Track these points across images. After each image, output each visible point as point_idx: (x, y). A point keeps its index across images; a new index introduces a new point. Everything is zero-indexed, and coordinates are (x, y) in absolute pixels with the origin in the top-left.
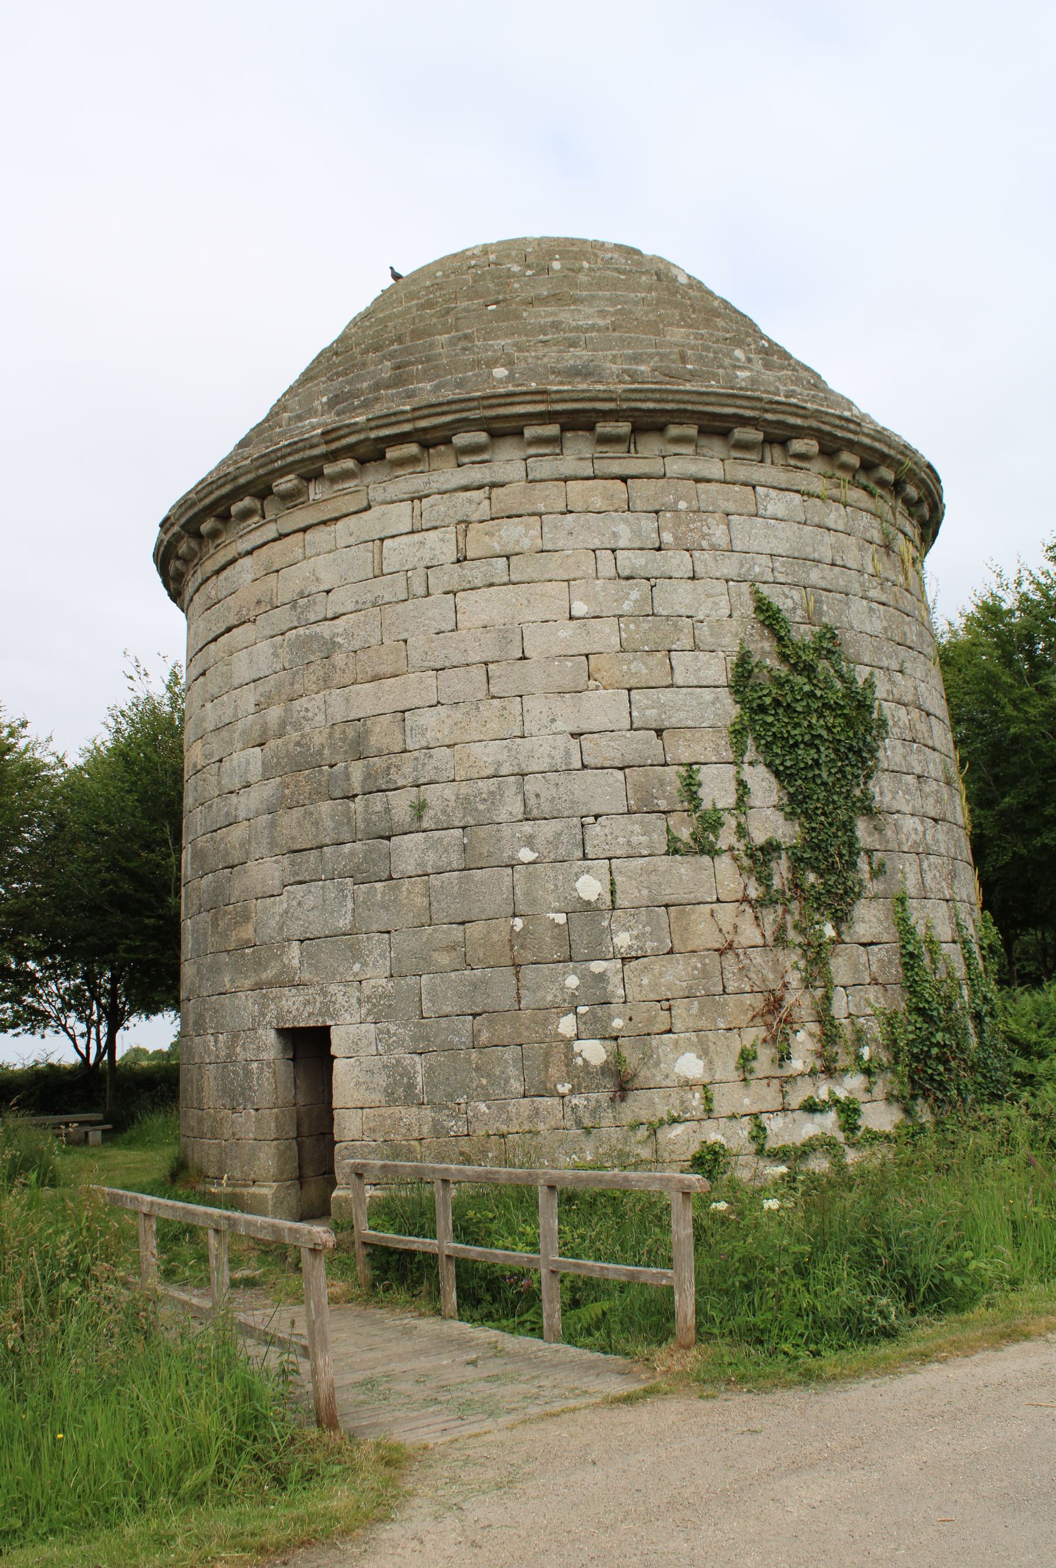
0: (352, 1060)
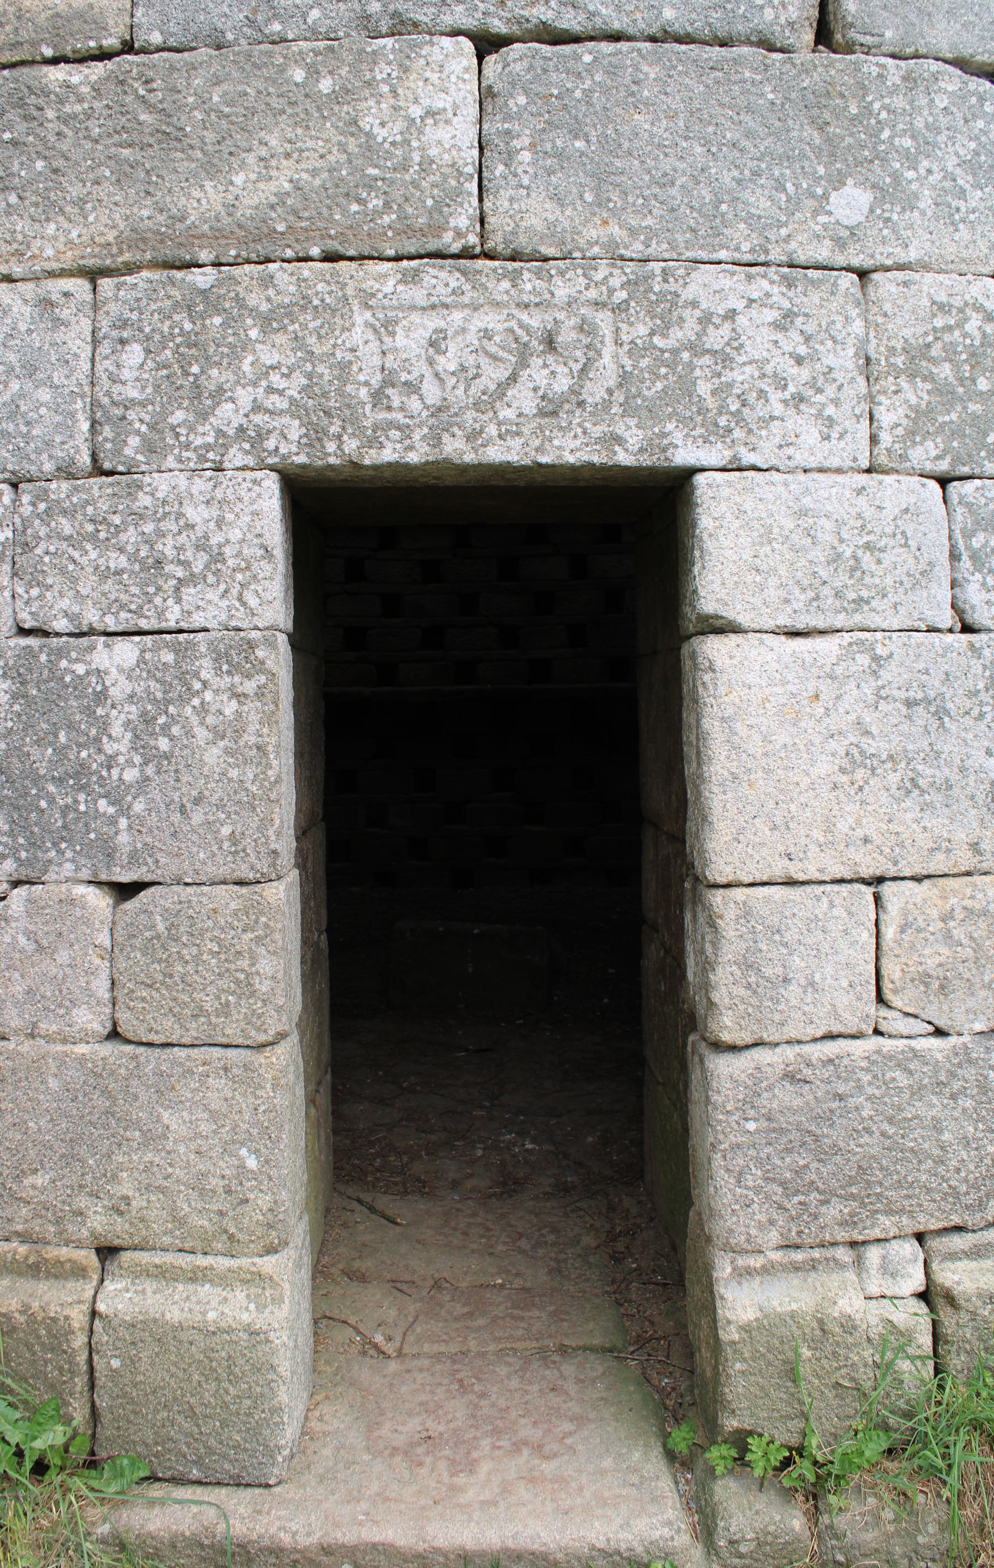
0: (827, 647)
